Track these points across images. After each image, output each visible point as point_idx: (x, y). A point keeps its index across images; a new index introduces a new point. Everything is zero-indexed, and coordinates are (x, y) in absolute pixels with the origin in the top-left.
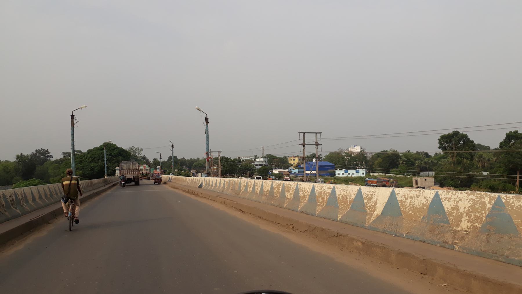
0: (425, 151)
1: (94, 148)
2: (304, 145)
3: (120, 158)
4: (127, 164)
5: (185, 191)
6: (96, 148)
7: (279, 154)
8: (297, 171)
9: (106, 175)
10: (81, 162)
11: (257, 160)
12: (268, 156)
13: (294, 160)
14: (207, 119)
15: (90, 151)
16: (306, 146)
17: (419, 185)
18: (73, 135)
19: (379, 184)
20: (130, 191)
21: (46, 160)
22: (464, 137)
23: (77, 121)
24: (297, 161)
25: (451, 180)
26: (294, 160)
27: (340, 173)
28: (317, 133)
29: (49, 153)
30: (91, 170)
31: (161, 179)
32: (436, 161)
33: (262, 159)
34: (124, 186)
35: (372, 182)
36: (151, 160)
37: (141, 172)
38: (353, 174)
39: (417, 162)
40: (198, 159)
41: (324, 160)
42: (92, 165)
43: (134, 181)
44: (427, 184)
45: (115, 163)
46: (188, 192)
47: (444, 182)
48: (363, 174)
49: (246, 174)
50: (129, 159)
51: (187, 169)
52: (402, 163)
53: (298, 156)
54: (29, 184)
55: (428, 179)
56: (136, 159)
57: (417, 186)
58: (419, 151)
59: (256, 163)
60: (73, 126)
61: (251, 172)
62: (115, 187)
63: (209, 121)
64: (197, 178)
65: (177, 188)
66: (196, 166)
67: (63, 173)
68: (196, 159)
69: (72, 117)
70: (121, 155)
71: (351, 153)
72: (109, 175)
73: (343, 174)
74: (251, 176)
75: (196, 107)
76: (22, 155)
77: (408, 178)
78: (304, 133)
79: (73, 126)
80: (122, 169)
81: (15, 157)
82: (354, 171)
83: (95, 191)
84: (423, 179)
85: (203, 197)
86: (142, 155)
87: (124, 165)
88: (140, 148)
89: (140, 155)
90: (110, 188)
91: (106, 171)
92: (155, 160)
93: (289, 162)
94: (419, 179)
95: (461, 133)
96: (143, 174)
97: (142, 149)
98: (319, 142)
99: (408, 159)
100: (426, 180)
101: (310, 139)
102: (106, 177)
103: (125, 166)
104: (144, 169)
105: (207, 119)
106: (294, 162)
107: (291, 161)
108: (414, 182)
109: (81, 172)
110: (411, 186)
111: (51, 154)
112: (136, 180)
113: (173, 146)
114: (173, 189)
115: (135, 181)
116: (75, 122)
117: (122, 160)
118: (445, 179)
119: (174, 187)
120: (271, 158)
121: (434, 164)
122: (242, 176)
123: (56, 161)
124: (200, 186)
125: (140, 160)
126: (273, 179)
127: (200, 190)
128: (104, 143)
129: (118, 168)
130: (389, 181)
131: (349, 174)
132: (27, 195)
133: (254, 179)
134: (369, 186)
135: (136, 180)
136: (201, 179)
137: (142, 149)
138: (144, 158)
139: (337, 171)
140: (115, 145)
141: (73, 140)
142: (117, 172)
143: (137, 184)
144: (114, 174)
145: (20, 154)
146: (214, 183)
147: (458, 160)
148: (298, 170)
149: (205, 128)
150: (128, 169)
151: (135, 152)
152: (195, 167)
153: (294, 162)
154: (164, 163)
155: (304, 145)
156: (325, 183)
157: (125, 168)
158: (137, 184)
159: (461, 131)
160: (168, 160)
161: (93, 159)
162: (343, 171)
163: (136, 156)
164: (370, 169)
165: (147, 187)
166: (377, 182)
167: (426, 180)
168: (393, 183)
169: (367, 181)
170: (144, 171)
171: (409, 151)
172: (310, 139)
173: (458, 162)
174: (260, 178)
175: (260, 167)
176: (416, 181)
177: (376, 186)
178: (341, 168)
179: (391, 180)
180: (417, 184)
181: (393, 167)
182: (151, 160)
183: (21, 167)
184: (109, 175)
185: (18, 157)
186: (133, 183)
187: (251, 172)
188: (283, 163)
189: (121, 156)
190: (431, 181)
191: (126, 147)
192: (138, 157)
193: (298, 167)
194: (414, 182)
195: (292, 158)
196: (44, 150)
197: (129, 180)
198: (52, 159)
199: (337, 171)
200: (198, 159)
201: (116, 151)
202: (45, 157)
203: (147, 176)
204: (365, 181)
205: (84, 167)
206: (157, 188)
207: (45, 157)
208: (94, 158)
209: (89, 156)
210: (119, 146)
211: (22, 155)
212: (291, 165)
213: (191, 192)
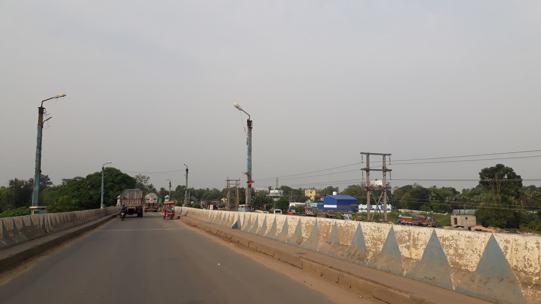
0: (452, 187)
2: (368, 170)
3: (123, 186)
5: (209, 232)
6: (97, 173)
7: (295, 186)
8: (315, 205)
10: (78, 189)
11: (271, 191)
12: (283, 188)
13: (311, 192)
14: (249, 123)
15: (89, 177)
16: (370, 172)
17: (459, 224)
18: (40, 139)
19: (414, 222)
21: (46, 187)
22: (509, 171)
23: (48, 117)
24: (314, 193)
25: (496, 220)
26: (311, 192)
28: (384, 155)
29: (49, 179)
30: (89, 199)
31: (173, 211)
32: (468, 198)
33: (277, 191)
34: (123, 218)
35: (406, 219)
36: (158, 190)
37: (147, 202)
39: (447, 198)
40: (208, 189)
41: (341, 194)
42: (91, 193)
43: (136, 212)
44: (468, 223)
45: (117, 191)
46: (216, 235)
47: (487, 222)
49: (263, 207)
50: (133, 187)
51: (196, 200)
52: (432, 199)
53: (314, 188)
54: (18, 213)
55: (469, 217)
56: (142, 187)
57: (456, 225)
58: (446, 187)
59: (271, 195)
60: (41, 125)
61: (269, 204)
63: (254, 125)
64: (208, 210)
65: (196, 226)
66: (205, 197)
67: (57, 201)
68: (205, 189)
69: (41, 110)
70: (125, 182)
71: (372, 186)
72: (107, 204)
74: (268, 209)
75: (235, 104)
76: (16, 180)
77: (444, 216)
78: (368, 154)
79: (41, 125)
80: (125, 198)
81: (9, 182)
83: (39, 242)
84: (464, 217)
85: (255, 250)
86: (149, 184)
87: (127, 193)
89: (146, 184)
90: (108, 220)
91: (102, 200)
92: (162, 189)
93: (306, 195)
94: (459, 218)
95: (506, 166)
97: (149, 178)
98: (388, 167)
99: (437, 194)
100: (466, 218)
101: (376, 162)
102: (102, 207)
104: (150, 198)
105: (249, 123)
107: (308, 194)
108: (453, 221)
109: (77, 200)
110: (450, 225)
111: (51, 181)
112: (139, 211)
113: (187, 170)
114: (188, 227)
115: (138, 212)
116: (45, 118)
117: (126, 188)
118: (488, 218)
119: (189, 224)
120: (286, 190)
121: (464, 200)
122: (258, 209)
123: (55, 189)
124: (236, 226)
125: (146, 189)
126: (294, 214)
127: (235, 233)
130: (426, 219)
133: (272, 212)
134: (402, 224)
135: (139, 211)
136: (211, 213)
137: (149, 178)
138: (151, 187)
139: (361, 206)
140: (119, 171)
141: (39, 147)
143: (140, 215)
144: (115, 203)
145: (14, 179)
147: (502, 197)
148: (317, 204)
149: (247, 136)
150: (129, 199)
151: (141, 181)
152: (205, 198)
154: (172, 192)
155: (368, 170)
156: (353, 220)
158: (140, 215)
159: (507, 164)
160: (176, 189)
161: (92, 186)
163: (142, 185)
164: (396, 205)
165: (155, 222)
166: (413, 220)
167: (466, 218)
168: (431, 221)
169: (400, 218)
170: (151, 201)
171: (435, 186)
172: (376, 162)
173: (503, 200)
174: (279, 212)
175: (279, 199)
176: (456, 219)
177: (411, 225)
179: (429, 218)
180: (456, 223)
181: (426, 203)
182: (158, 190)
183: (13, 194)
184: (107, 204)
185: (12, 182)
186: (136, 215)
187: (269, 204)
188: (299, 195)
189: (125, 183)
190: (472, 220)
191: (132, 175)
192: (144, 186)
193: (317, 199)
194: (453, 221)
197: (131, 211)
198: (51, 186)
200: (208, 189)
201: (119, 177)
202: (45, 183)
203: (154, 208)
204: (398, 218)
205: (81, 194)
206: (169, 226)
207: (45, 183)
208: (94, 185)
209: (88, 182)
211: (16, 180)
212: (309, 198)
213: (222, 235)
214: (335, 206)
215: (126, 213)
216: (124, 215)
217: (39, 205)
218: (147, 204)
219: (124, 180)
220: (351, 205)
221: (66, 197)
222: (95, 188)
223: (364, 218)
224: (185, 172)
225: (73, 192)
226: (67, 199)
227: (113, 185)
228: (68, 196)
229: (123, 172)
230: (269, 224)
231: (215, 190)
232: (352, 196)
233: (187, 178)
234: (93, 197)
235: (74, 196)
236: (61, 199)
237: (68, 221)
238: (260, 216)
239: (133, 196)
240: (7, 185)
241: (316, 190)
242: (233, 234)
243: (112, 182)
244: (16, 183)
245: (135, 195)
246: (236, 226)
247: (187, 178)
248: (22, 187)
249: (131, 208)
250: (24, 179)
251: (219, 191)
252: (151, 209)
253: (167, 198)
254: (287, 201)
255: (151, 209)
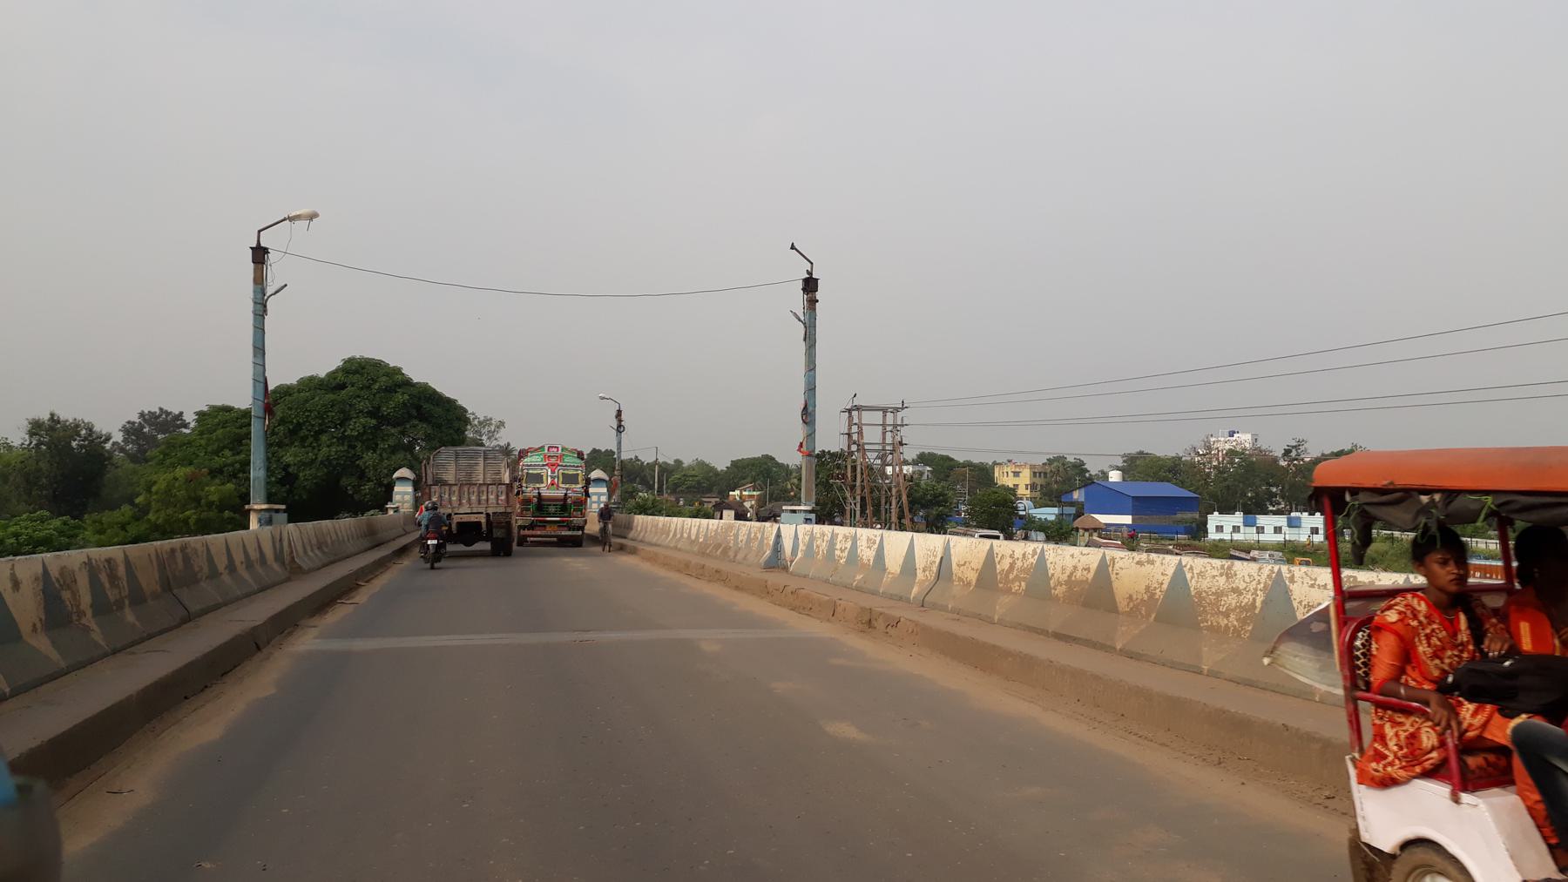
1: (302, 382)
4: (462, 462)
6: (311, 379)
9: (258, 504)
13: (1016, 474)
20: (478, 578)
24: (1025, 478)
26: (1016, 474)
27: (1223, 525)
34: (435, 558)
37: (530, 491)
38: (1278, 530)
42: (288, 458)
48: (1315, 531)
62: (406, 562)
67: (149, 490)
70: (423, 417)
73: (1236, 529)
81: (25, 426)
82: (1281, 521)
88: (496, 418)
89: (494, 443)
90: (381, 565)
96: (541, 505)
97: (502, 424)
103: (452, 468)
106: (1016, 481)
109: (230, 486)
112: (498, 533)
113: (810, 285)
115: (494, 538)
127: (775, 578)
128: (350, 361)
129: (404, 472)
131: (1260, 530)
132: (213, 551)
135: (498, 533)
137: (502, 424)
139: (1214, 520)
140: (398, 371)
142: (403, 493)
145: (45, 417)
146: (694, 531)
148: (1056, 510)
153: (1016, 481)
157: (450, 477)
158: (502, 549)
162: (1238, 518)
178: (1227, 509)
185: (36, 427)
186: (487, 546)
195: (1009, 469)
196: (168, 414)
197: (469, 532)
199: (1214, 520)
200: (678, 462)
201: (400, 397)
208: (299, 425)
210: (416, 373)
214: (1127, 519)
215: (447, 538)
216: (437, 547)
217: (269, 502)
218: (527, 502)
219: (419, 408)
220: (1179, 516)
221: (181, 472)
222: (303, 439)
223: (1222, 551)
224: (798, 299)
225: (217, 452)
226: (189, 480)
227: (377, 428)
228: (189, 470)
229: (416, 378)
230: (894, 562)
231: (702, 465)
232: (1182, 484)
233: (810, 338)
234: (296, 477)
235: (215, 473)
236: (162, 480)
237: (137, 598)
238: (864, 540)
239: (470, 475)
240: (18, 437)
241: (1032, 467)
242: (711, 565)
243: (371, 414)
244: (52, 429)
245: (481, 468)
246: (776, 561)
247: (810, 338)
248: (74, 444)
249: (466, 519)
250: (79, 418)
251: (713, 469)
252: (549, 530)
253: (598, 480)
254: (949, 496)
255: (549, 530)
